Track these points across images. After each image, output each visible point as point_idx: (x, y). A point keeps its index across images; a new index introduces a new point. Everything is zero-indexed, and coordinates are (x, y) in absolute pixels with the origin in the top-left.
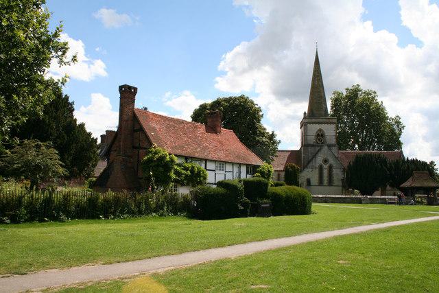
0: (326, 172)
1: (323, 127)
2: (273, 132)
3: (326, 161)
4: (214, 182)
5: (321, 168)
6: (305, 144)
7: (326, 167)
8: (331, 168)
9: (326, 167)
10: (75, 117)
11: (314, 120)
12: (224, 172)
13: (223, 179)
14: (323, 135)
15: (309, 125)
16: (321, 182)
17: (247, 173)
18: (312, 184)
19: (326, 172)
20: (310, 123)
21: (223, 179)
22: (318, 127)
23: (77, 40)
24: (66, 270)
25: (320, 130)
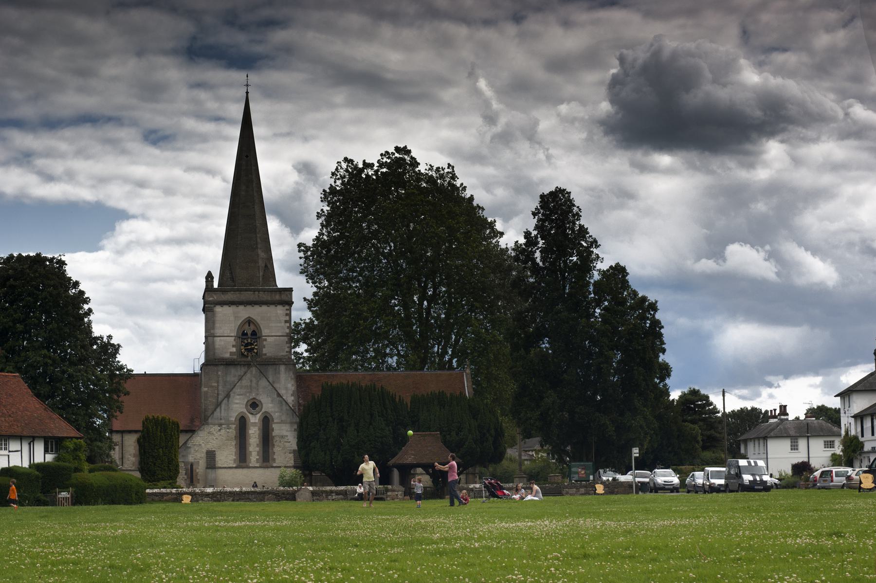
0: (254, 433)
3: (254, 405)
4: (218, 332)
5: (242, 424)
6: (212, 361)
7: (254, 420)
8: (266, 421)
9: (254, 420)
10: (749, 408)
11: (230, 296)
12: (6, 452)
13: (42, 461)
15: (218, 309)
17: (46, 451)
18: (210, 471)
19: (254, 433)
20: (222, 303)
21: (42, 461)
22: (245, 312)
23: (818, 407)
24: (820, 405)
25: (249, 321)
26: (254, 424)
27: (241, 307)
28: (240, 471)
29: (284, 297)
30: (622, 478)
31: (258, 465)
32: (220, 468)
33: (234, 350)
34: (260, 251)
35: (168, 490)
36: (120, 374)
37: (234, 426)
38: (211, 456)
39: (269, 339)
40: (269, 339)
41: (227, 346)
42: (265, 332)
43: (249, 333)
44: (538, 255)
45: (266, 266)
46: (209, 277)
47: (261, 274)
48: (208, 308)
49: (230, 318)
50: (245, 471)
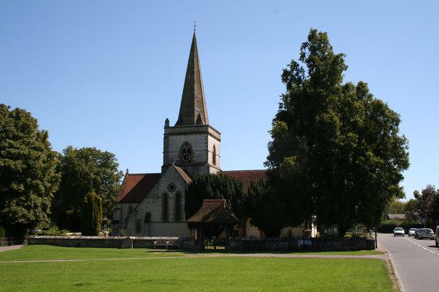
0: (172, 203)
1: (191, 139)
2: (317, 42)
3: (172, 187)
5: (165, 197)
7: (172, 195)
8: (178, 196)
9: (172, 195)
14: (190, 151)
16: (165, 218)
19: (172, 203)
20: (172, 134)
25: (186, 143)
26: (172, 198)
27: (182, 136)
28: (163, 224)
29: (204, 129)
30: (338, 123)
31: (173, 221)
32: (149, 226)
33: (178, 159)
34: (196, 107)
35: (49, 237)
36: (311, 219)
37: (160, 199)
38: (148, 216)
39: (196, 153)
40: (196, 153)
41: (175, 155)
42: (194, 149)
43: (186, 149)
44: (376, 159)
45: (199, 116)
46: (167, 121)
47: (196, 119)
48: (166, 137)
49: (179, 140)
50: (166, 224)
